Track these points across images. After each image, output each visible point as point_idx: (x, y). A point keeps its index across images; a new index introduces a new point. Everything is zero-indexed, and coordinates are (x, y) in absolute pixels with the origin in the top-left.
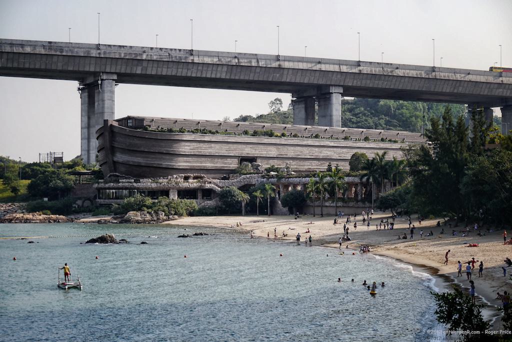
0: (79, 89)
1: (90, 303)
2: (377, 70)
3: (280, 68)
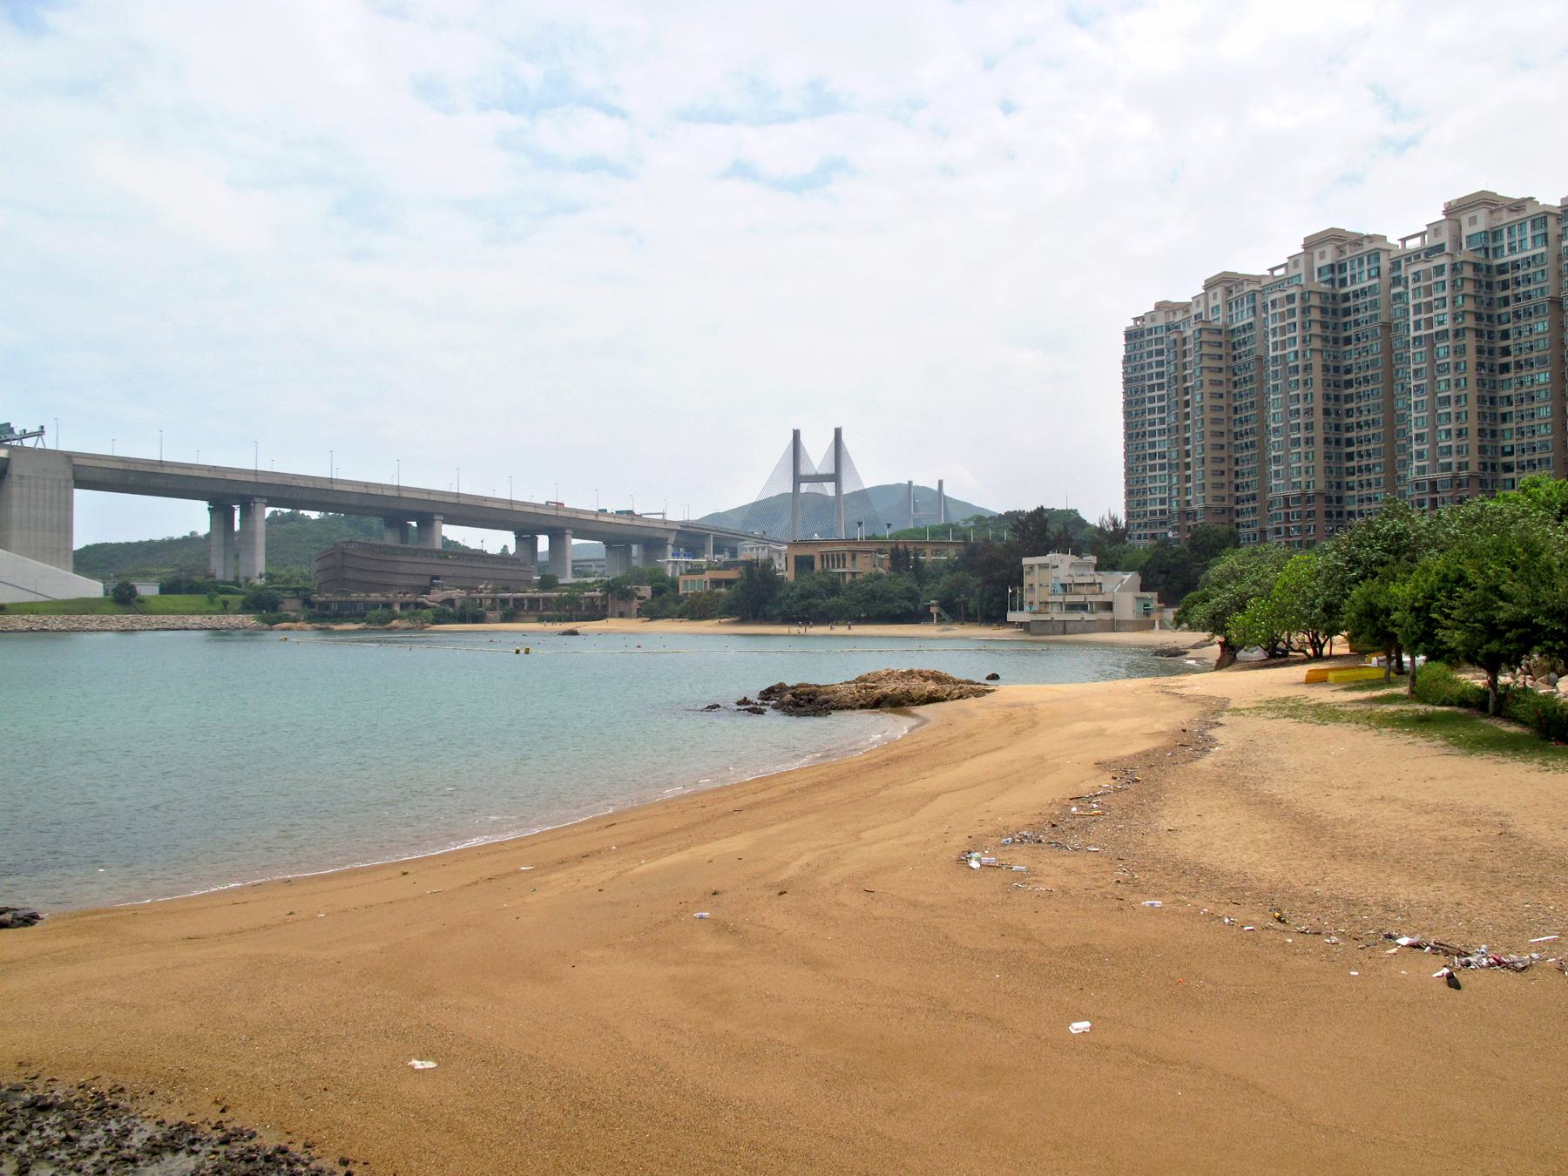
0: (209, 509)
1: (95, 752)
2: (470, 502)
3: (399, 498)
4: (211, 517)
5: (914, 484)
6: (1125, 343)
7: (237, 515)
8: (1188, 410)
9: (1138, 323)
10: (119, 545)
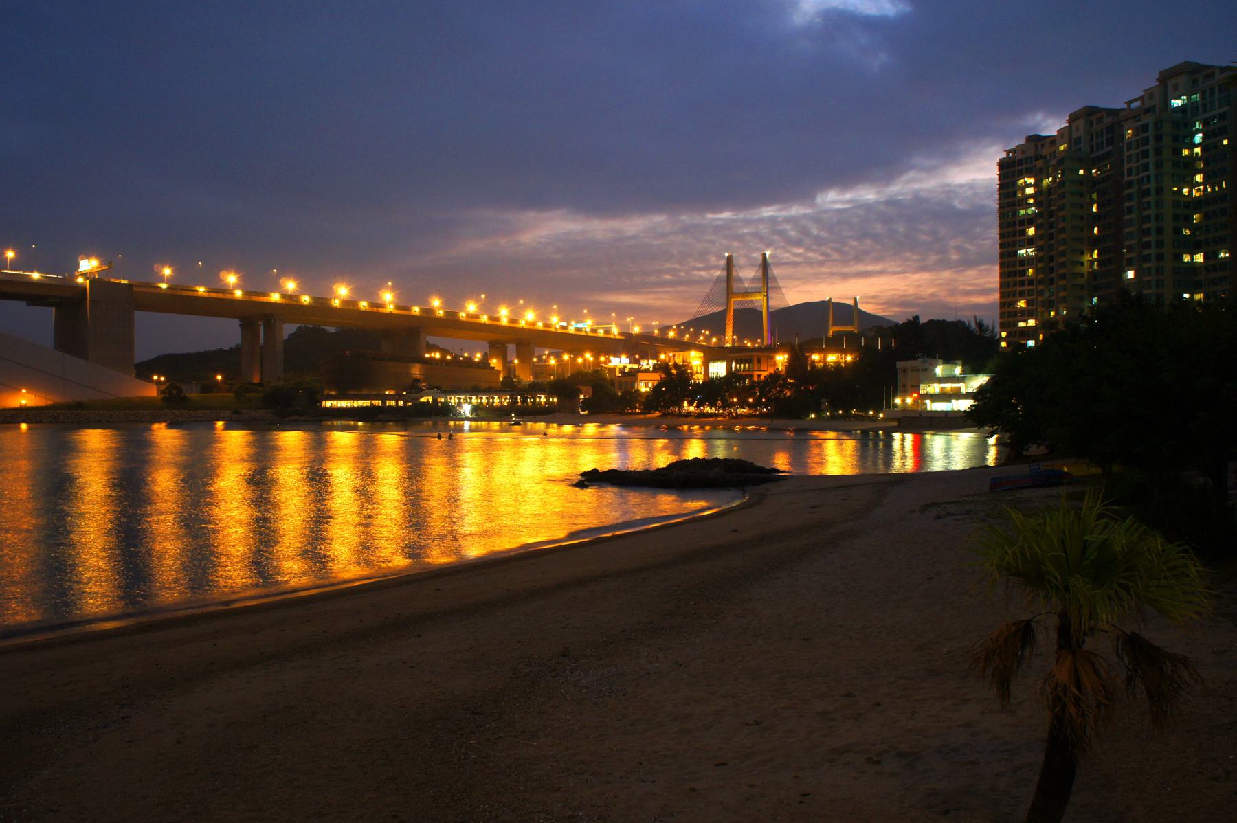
4: (242, 332)
5: (833, 301)
6: (998, 173)
7: (262, 329)
8: (1053, 231)
9: (1010, 155)
10: (183, 355)
